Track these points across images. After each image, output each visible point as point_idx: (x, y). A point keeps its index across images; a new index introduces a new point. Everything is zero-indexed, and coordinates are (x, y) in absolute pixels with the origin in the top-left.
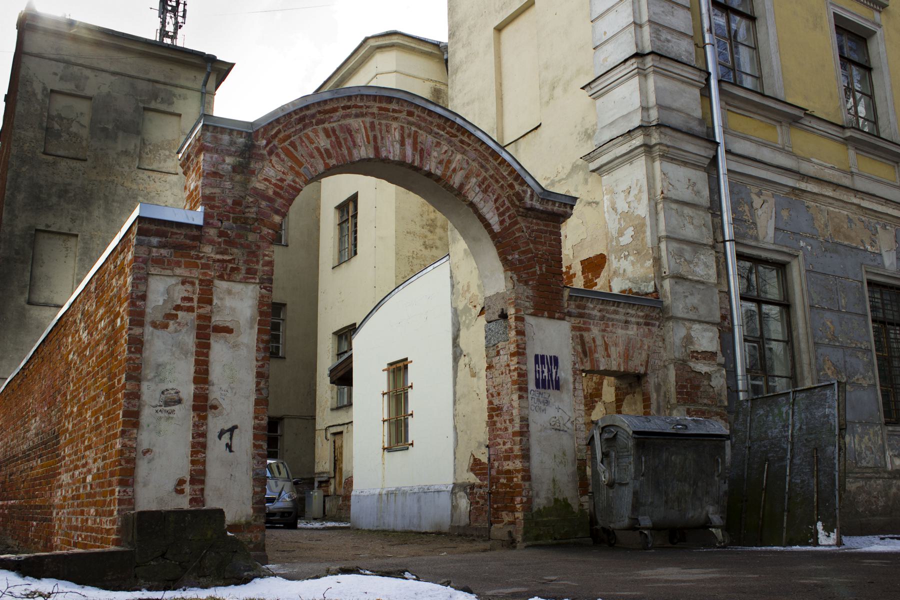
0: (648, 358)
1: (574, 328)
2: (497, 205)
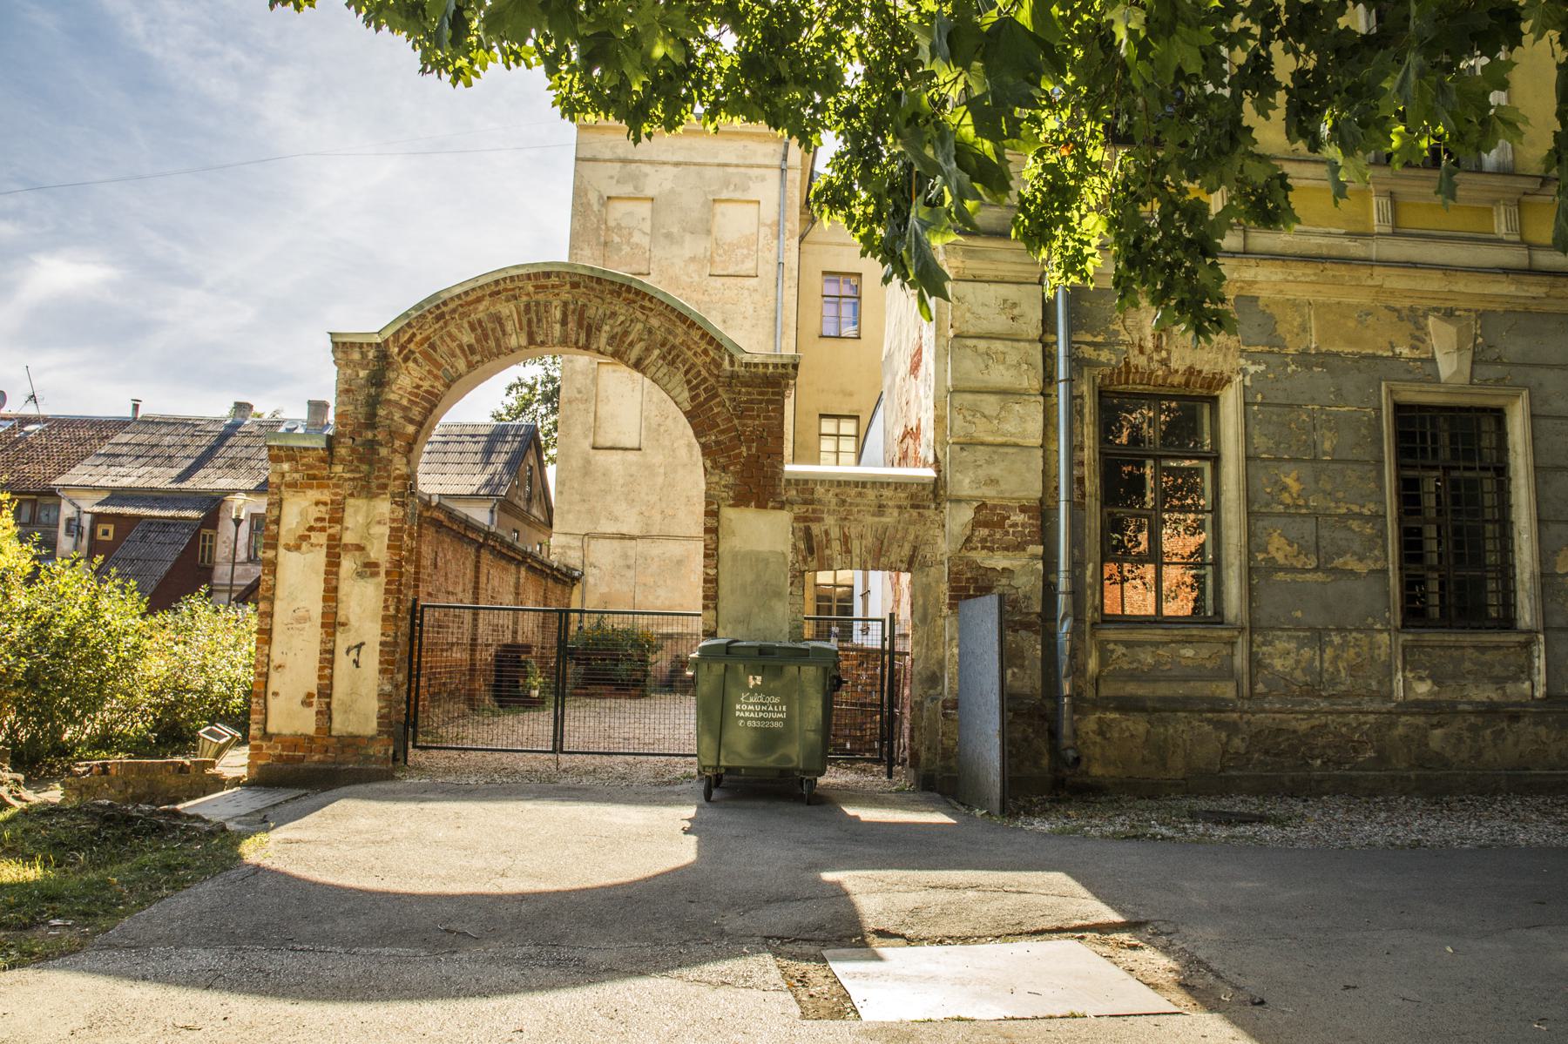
0: (914, 551)
1: (797, 519)
2: (689, 376)
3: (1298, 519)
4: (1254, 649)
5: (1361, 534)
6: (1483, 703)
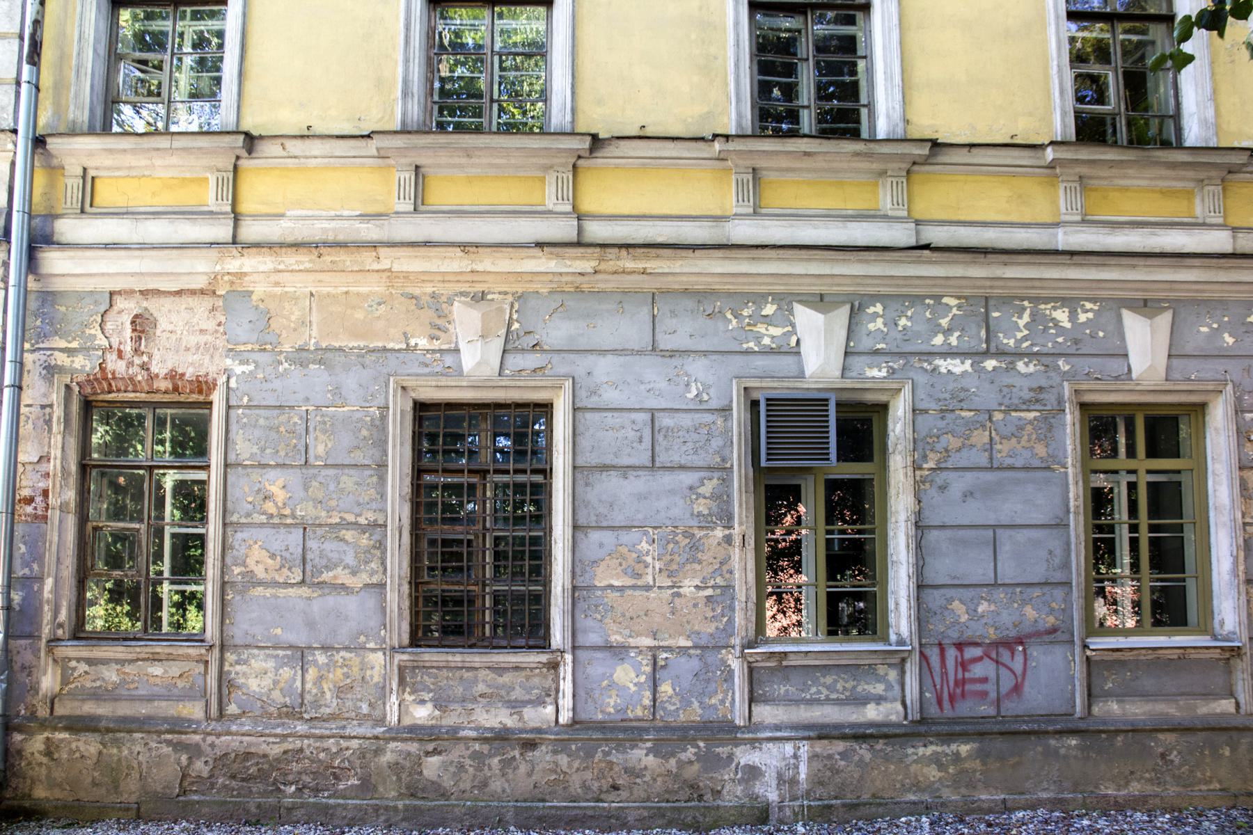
3: (282, 530)
4: (226, 668)
5: (356, 545)
6: (492, 729)
